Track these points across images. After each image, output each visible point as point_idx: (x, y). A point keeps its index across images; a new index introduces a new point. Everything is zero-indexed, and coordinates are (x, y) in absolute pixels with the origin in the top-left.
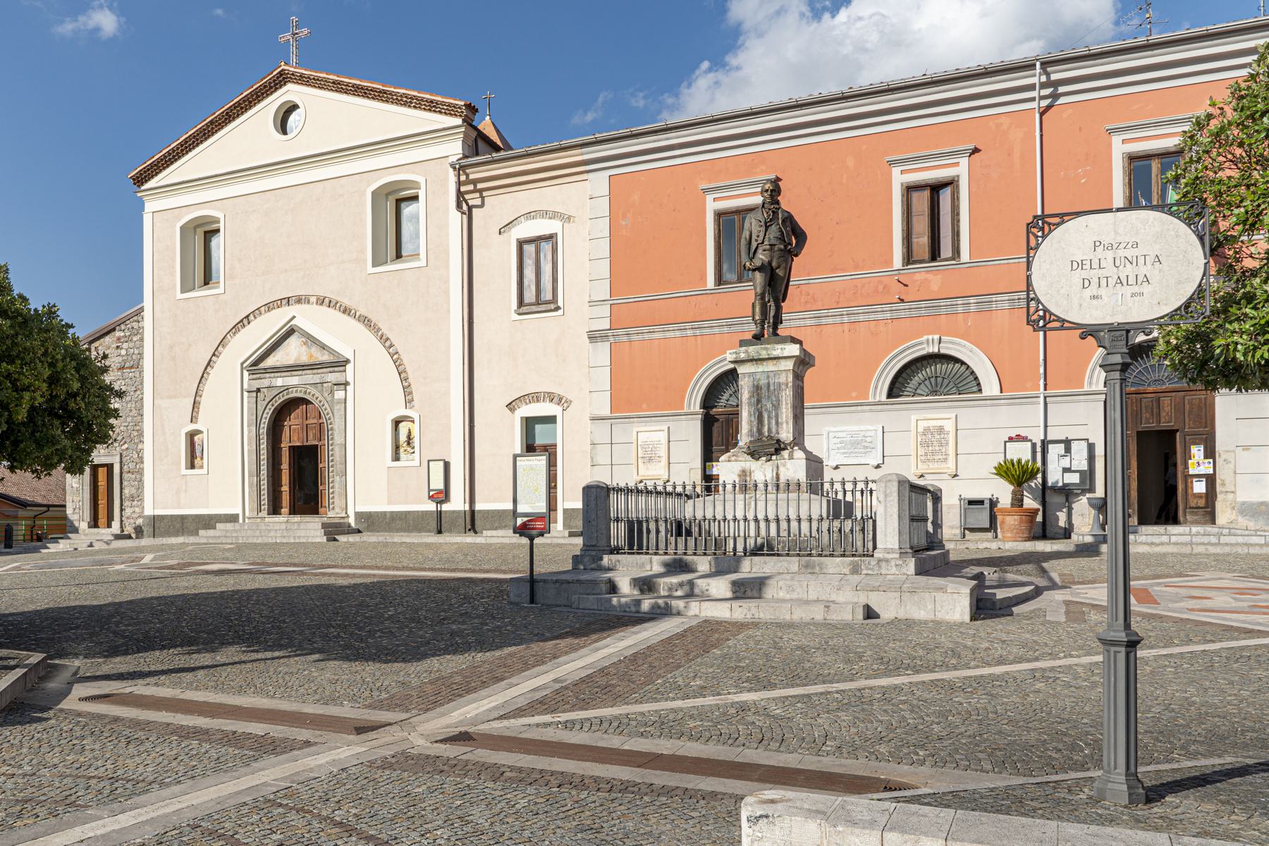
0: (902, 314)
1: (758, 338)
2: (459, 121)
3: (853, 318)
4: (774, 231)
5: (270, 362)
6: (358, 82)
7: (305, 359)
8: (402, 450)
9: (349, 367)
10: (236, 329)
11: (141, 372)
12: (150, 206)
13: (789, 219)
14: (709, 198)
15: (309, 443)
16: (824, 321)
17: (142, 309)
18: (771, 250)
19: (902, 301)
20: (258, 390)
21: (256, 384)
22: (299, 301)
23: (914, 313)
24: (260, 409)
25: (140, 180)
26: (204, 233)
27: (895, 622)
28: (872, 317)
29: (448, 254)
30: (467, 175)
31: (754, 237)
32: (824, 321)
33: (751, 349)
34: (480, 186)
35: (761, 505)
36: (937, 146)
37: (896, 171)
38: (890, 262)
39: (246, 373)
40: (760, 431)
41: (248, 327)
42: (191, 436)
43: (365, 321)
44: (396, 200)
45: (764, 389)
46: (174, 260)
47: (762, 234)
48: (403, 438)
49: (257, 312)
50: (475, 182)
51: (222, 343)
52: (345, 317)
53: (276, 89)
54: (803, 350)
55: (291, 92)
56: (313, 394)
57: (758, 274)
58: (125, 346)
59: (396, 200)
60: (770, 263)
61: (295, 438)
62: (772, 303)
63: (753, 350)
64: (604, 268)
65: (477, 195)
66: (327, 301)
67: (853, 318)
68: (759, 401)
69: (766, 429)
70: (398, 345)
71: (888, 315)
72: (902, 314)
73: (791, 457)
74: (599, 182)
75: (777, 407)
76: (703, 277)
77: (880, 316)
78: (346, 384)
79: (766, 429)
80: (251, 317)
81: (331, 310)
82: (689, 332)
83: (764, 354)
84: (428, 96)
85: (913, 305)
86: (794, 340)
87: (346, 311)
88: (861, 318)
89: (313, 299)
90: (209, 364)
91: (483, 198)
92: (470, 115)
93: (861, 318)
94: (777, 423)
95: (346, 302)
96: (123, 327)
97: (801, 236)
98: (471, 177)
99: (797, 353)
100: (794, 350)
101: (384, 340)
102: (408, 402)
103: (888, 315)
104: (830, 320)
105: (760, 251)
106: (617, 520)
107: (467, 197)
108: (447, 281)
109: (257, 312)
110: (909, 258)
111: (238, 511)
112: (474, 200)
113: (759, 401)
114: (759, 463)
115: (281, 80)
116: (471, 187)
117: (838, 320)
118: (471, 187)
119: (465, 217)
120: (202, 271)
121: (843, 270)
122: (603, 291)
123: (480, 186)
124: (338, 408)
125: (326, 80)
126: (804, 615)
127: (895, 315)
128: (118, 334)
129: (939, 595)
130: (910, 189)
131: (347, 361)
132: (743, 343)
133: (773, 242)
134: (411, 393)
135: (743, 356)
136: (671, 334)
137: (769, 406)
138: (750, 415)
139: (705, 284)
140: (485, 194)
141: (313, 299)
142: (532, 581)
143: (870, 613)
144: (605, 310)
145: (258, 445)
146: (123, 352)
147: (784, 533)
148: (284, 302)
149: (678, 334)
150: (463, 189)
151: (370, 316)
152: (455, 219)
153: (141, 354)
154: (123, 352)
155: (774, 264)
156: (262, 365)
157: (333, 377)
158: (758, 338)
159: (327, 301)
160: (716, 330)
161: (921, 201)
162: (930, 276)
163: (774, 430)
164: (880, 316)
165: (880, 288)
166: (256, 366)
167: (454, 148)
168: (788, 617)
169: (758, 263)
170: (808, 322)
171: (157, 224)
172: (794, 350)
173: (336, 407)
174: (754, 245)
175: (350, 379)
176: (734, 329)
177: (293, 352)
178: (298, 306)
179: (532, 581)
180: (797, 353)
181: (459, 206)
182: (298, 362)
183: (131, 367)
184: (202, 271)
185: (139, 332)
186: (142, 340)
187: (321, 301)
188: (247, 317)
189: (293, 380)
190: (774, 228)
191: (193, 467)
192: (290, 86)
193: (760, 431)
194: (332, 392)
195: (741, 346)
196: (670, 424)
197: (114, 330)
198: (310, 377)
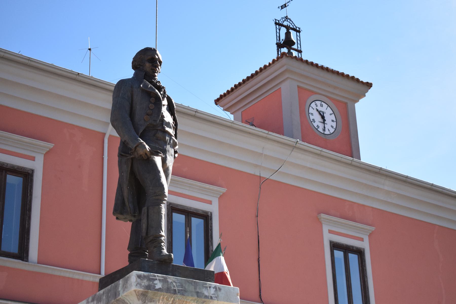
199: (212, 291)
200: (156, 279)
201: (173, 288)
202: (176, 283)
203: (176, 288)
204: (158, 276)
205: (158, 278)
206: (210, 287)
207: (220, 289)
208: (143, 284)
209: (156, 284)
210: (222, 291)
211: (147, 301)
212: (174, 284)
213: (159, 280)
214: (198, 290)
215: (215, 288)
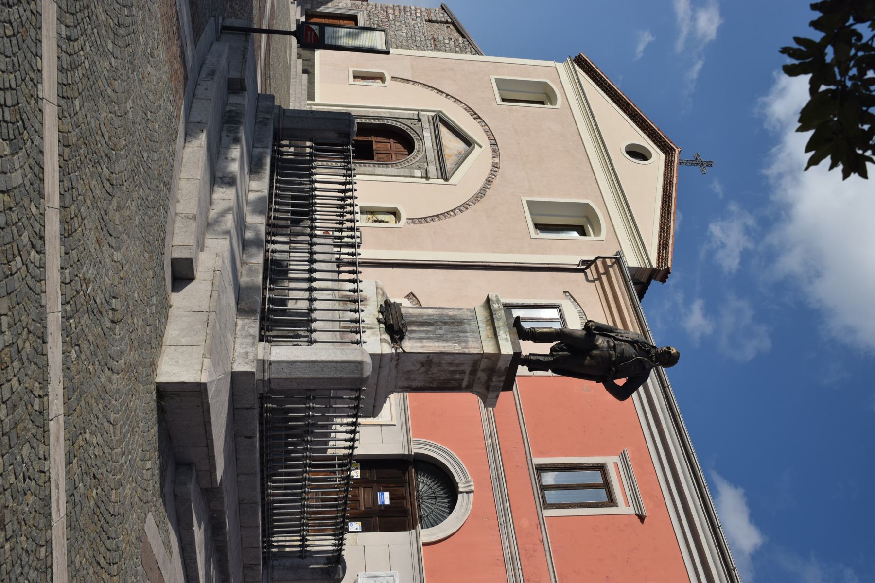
2: (655, 266)
5: (444, 131)
6: (674, 196)
7: (446, 152)
8: (370, 216)
9: (442, 181)
10: (469, 109)
11: (432, 50)
12: (560, 66)
14: (617, 459)
15: (375, 155)
16: (509, 567)
17: (478, 53)
20: (419, 120)
21: (424, 120)
22: (494, 151)
24: (404, 121)
25: (580, 61)
26: (543, 96)
27: (165, 306)
29: (542, 253)
30: (612, 266)
34: (604, 278)
35: (329, 315)
36: (733, 555)
39: (433, 114)
40: (412, 323)
41: (472, 118)
42: (381, 78)
43: (480, 195)
44: (582, 222)
45: (460, 329)
46: (520, 76)
48: (381, 217)
49: (484, 124)
50: (607, 273)
51: (457, 100)
52: (483, 180)
53: (658, 146)
55: (658, 157)
56: (416, 157)
58: (452, 43)
59: (582, 222)
61: (379, 145)
65: (596, 277)
66: (496, 169)
68: (445, 323)
69: (414, 328)
70: (460, 216)
73: (382, 340)
75: (440, 338)
78: (427, 178)
79: (414, 328)
80: (479, 120)
81: (488, 171)
82: (489, 442)
84: (671, 242)
87: (489, 181)
89: (497, 160)
90: (439, 91)
91: (594, 281)
92: (660, 275)
94: (422, 338)
95: (496, 182)
96: (466, 43)
98: (611, 269)
101: (466, 206)
102: (413, 220)
104: (510, 573)
106: (311, 300)
107: (592, 267)
108: (519, 252)
109: (484, 124)
111: (317, 101)
112: (591, 272)
113: (445, 323)
114: (376, 313)
115: (667, 149)
116: (602, 270)
118: (602, 270)
119: (576, 267)
120: (515, 93)
123: (604, 278)
124: (407, 172)
125: (672, 176)
126: (184, 192)
128: (461, 40)
129: (200, 350)
131: (446, 180)
133: (618, 349)
134: (421, 223)
136: (486, 426)
137: (441, 332)
138: (429, 315)
140: (597, 282)
141: (497, 160)
142: (248, 31)
143: (182, 274)
145: (374, 118)
146: (447, 41)
147: (293, 285)
148: (493, 142)
149: (487, 432)
150: (599, 262)
151: (485, 197)
152: (574, 260)
153: (446, 51)
154: (447, 41)
156: (440, 125)
157: (432, 170)
159: (496, 169)
160: (493, 466)
163: (413, 335)
166: (440, 120)
167: (632, 260)
168: (183, 175)
170: (507, 552)
171: (547, 69)
173: (407, 170)
175: (431, 181)
176: (496, 482)
177: (452, 145)
178: (490, 151)
179: (248, 31)
181: (584, 262)
182: (444, 149)
183: (435, 45)
184: (515, 93)
185: (463, 51)
186: (457, 53)
187: (495, 166)
188: (479, 118)
189: (429, 142)
191: (355, 77)
192: (662, 156)
193: (412, 323)
194: (419, 168)
196: (398, 426)
197: (463, 37)
198: (431, 154)
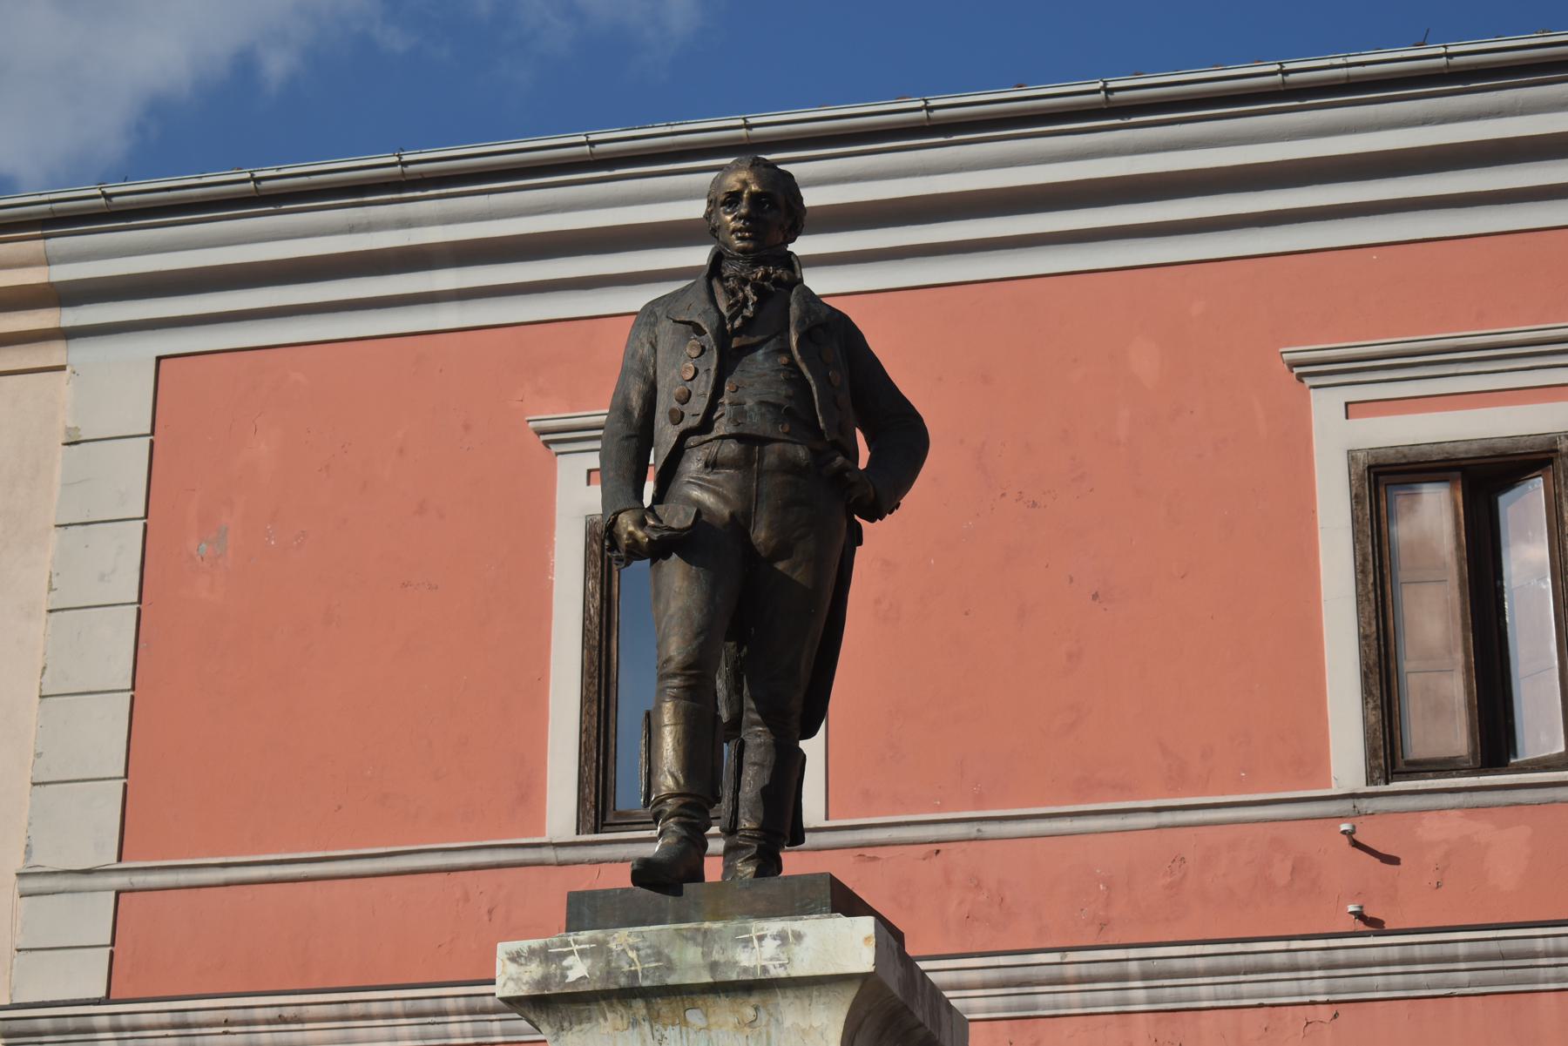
0: (1377, 983)
1: (668, 880)
3: (1169, 994)
4: (759, 377)
13: (834, 334)
16: (1045, 1000)
18: (743, 463)
19: (1375, 926)
23: (1425, 980)
28: (1251, 989)
31: (664, 403)
32: (1045, 1000)
33: (621, 938)
37: (1326, 405)
38: (1316, 761)
47: (704, 386)
54: (890, 936)
57: (676, 574)
60: (739, 524)
62: (757, 738)
63: (631, 947)
64: (102, 735)
67: (1169, 994)
71: (1318, 987)
72: (1377, 983)
74: (112, 381)
76: (530, 793)
77: (1283, 988)
83: (690, 965)
85: (1421, 946)
86: (846, 903)
88: (1205, 993)
93: (1205, 993)
97: (903, 439)
99: (863, 960)
100: (847, 945)
103: (1318, 987)
104: (1072, 999)
105: (693, 465)
110: (1389, 756)
117: (1104, 997)
121: (1123, 790)
122: (89, 830)
127: (1346, 985)
130: (1384, 479)
132: (586, 911)
133: (757, 423)
135: (578, 970)
139: (537, 818)
144: (91, 916)
155: (760, 534)
158: (668, 880)
161: (1432, 515)
162: (1482, 829)
164: (1283, 988)
165: (1281, 872)
169: (677, 517)
172: (847, 945)
174: (666, 434)
180: (863, 960)
190: (760, 364)
195: (575, 922)
199: (770, 946)
200: (572, 953)
201: (626, 968)
202: (638, 950)
203: (639, 968)
204: (576, 942)
205: (575, 948)
206: (761, 938)
207: (798, 937)
208: (526, 977)
209: (569, 968)
210: (807, 942)
211: (566, 1024)
212: (632, 954)
213: (582, 953)
214: (716, 956)
215: (782, 937)
